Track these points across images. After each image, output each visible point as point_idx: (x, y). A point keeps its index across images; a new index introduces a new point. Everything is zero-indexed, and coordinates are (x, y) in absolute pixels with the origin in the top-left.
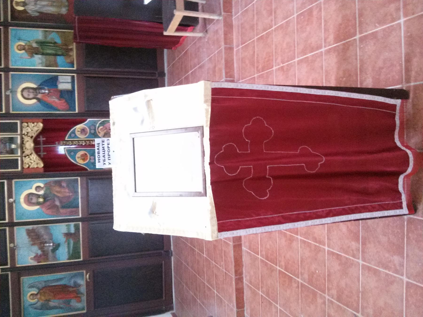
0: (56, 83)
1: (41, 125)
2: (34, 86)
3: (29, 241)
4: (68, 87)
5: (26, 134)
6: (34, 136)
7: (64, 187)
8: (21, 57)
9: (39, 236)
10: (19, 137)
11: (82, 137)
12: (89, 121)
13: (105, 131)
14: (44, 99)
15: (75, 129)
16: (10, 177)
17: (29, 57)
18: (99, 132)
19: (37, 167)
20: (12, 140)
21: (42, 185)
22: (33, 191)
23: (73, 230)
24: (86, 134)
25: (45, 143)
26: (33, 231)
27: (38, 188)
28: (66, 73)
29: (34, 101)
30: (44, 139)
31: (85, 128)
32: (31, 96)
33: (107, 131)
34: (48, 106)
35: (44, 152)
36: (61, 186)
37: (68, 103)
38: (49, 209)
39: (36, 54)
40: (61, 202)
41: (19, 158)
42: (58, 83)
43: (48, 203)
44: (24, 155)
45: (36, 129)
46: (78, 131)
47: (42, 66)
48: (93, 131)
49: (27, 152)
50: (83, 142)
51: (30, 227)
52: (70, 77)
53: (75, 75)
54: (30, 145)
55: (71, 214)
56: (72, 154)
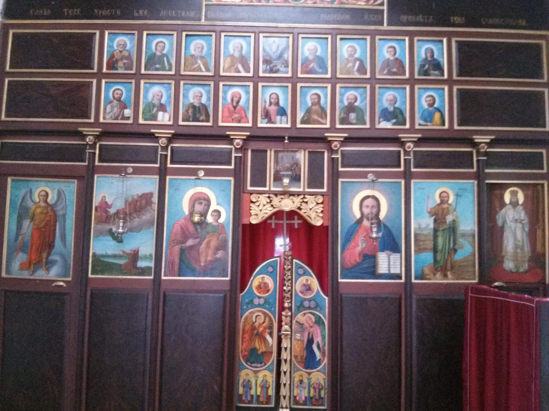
0: (387, 249)
1: (319, 223)
2: (382, 216)
3: (133, 196)
4: (382, 269)
5: (305, 200)
6: (301, 212)
8: (428, 198)
9: (139, 211)
10: (301, 190)
11: (298, 286)
12: (325, 299)
13: (307, 325)
15: (312, 276)
17: (429, 210)
18: (305, 314)
19: (251, 215)
20: (296, 179)
21: (221, 220)
22: (214, 206)
23: (141, 264)
24: (302, 292)
27: (218, 214)
29: (358, 215)
30: (296, 226)
32: (366, 211)
33: (306, 328)
35: (276, 224)
36: (218, 249)
37: (354, 266)
38: (182, 228)
39: (435, 221)
40: (191, 247)
41: (267, 189)
42: (388, 252)
44: (271, 195)
45: (313, 215)
46: (307, 280)
48: (306, 304)
49: (276, 200)
51: (155, 199)
52: (399, 272)
54: (286, 206)
55: (171, 264)
56: (270, 269)
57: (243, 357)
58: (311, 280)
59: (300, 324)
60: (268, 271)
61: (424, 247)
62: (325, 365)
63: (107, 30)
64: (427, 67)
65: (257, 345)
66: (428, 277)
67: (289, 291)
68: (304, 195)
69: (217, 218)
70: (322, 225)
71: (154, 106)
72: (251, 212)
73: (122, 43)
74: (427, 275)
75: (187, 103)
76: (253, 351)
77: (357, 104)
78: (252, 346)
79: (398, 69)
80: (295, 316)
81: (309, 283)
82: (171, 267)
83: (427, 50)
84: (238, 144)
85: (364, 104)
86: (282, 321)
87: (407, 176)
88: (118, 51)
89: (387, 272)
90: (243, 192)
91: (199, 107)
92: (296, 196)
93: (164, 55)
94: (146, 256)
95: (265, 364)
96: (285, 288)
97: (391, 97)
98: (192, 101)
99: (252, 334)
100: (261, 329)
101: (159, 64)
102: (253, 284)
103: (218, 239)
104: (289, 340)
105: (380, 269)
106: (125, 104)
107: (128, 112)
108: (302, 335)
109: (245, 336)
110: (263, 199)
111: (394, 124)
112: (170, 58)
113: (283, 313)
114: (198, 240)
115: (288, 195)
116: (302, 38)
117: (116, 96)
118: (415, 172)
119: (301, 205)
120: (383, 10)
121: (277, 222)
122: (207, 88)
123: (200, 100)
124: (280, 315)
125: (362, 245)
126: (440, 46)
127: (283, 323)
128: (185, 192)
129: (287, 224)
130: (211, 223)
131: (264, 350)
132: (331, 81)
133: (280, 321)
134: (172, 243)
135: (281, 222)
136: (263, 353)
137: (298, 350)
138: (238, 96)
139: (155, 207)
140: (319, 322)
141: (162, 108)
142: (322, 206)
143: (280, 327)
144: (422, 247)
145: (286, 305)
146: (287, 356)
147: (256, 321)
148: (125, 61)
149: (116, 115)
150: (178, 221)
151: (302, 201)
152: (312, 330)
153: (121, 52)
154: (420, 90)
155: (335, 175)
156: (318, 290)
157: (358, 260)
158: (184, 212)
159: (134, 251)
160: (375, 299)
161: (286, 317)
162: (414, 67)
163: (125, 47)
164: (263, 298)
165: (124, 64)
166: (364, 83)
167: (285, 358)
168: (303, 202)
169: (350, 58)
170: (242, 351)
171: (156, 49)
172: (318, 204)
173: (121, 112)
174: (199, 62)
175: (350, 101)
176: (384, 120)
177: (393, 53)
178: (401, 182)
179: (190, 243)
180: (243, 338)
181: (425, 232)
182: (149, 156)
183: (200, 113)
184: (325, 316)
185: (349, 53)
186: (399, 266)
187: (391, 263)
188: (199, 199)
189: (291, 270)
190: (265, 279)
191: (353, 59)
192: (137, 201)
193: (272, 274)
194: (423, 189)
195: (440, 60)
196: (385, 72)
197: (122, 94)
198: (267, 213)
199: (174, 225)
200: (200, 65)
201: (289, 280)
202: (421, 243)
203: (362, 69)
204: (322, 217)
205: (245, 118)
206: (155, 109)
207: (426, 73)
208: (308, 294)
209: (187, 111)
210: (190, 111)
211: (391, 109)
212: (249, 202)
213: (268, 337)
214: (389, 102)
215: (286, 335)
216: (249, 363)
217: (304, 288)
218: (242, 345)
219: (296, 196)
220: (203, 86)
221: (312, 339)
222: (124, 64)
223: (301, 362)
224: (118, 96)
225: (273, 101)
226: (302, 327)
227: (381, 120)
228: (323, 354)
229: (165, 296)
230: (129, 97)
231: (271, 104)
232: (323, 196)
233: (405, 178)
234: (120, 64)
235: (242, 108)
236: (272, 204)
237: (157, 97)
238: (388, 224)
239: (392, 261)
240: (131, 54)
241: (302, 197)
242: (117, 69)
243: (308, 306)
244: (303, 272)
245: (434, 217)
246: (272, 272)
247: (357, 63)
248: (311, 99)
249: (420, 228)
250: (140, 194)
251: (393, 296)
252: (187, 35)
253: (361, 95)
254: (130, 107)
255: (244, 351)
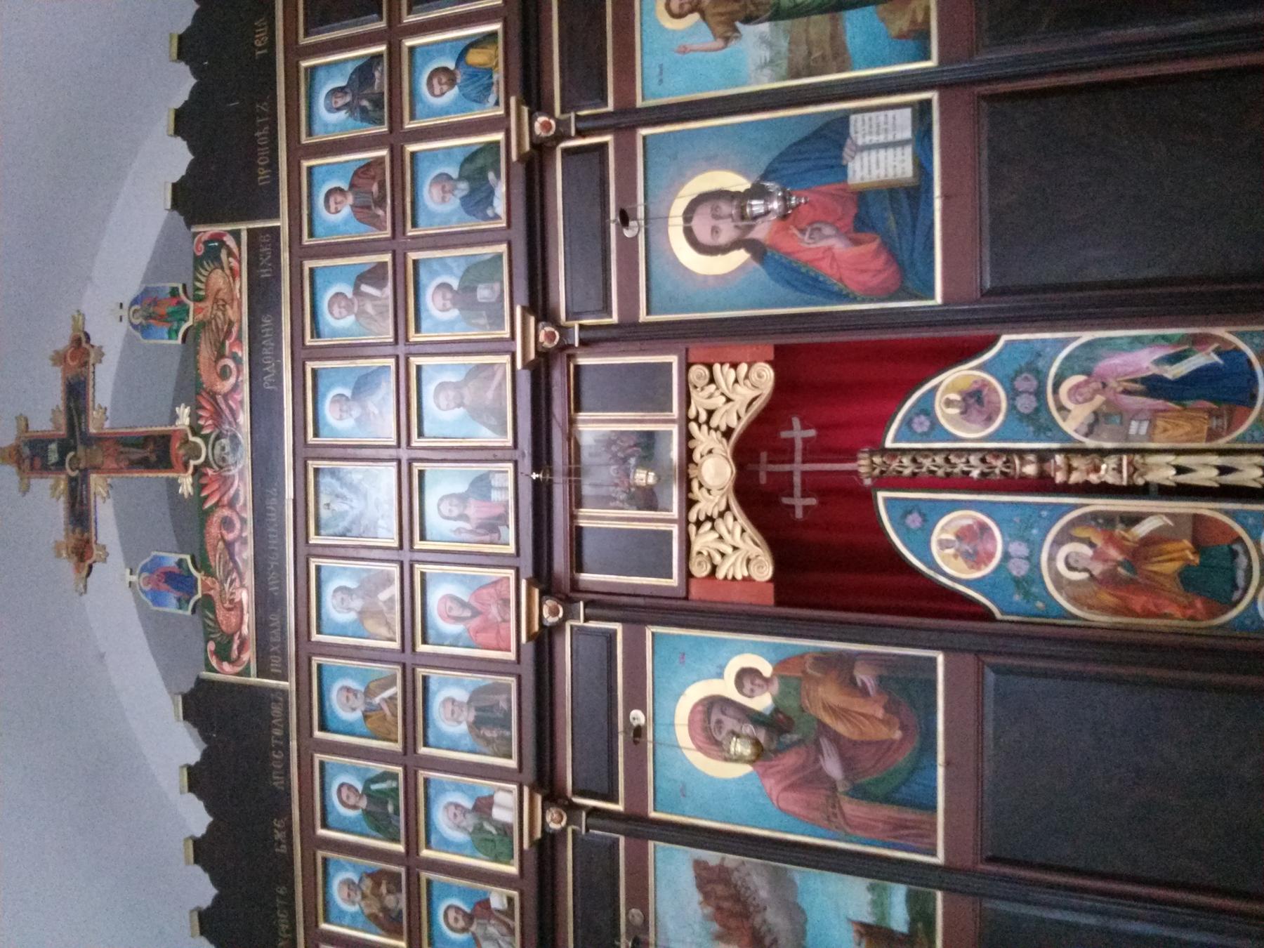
0: (840, 157)
1: (765, 375)
2: (738, 183)
3: (706, 917)
4: (899, 165)
5: (703, 417)
6: (739, 428)
7: (864, 692)
8: (684, 50)
9: (745, 905)
10: (675, 429)
11: (971, 435)
12: (1008, 343)
13: (1099, 399)
14: (786, 245)
15: (935, 388)
16: (641, 610)
17: (720, 43)
18: (1061, 408)
19: (748, 579)
20: (647, 445)
21: (767, 669)
22: (726, 687)
23: (899, 919)
24: (990, 420)
25: (813, 452)
26: (722, 875)
27: (746, 675)
28: (890, 92)
29: (740, 257)
30: (812, 433)
31: (985, 384)
32: (728, 233)
33: (1107, 402)
34: (804, 280)
35: (805, 494)
36: (851, 685)
37: (893, 256)
38: (792, 787)
39: (748, 20)
40: (848, 764)
41: (675, 529)
42: (847, 152)
43: (790, 760)
44: (693, 517)
45: (744, 393)
46: (949, 403)
47: (772, 80)
48: (1026, 404)
49: (707, 504)
50: (974, 459)
51: (712, 857)
52: (907, 112)
53: (933, 95)
54: (718, 473)
55: (899, 833)
56: (914, 521)
57: (1214, 615)
58: (947, 390)
59: (1096, 421)
60: (921, 529)
61: (827, 46)
62: (1230, 332)
63: (317, 926)
64: (365, 103)
65: (1171, 567)
66: (920, 18)
67: (983, 460)
68: (688, 420)
69: (758, 681)
70: (773, 364)
71: (479, 829)
72: (739, 577)
73: (346, 890)
74: (913, 22)
75: (468, 741)
76: (1187, 578)
77: (455, 284)
78: (1175, 587)
79: (373, 178)
80: (1070, 439)
81: (955, 397)
82: (906, 832)
83: (331, 110)
84: (554, 612)
85: (454, 265)
86: (1087, 483)
87: (628, 119)
88: (363, 904)
89: (908, 150)
90: (686, 598)
91: (478, 709)
92: (692, 444)
93: (367, 792)
94: (874, 903)
95: (1239, 540)
96: (975, 474)
97: (436, 192)
98: (464, 728)
99: (1129, 584)
100: (1114, 554)
101: (387, 803)
102: (964, 576)
103: (818, 682)
104: (1152, 459)
105: (899, 175)
106: (479, 903)
107: (498, 899)
108: (1136, 415)
109: (1138, 608)
110: (704, 541)
111: (498, 176)
112: (371, 775)
113: (1059, 478)
114: (824, 743)
115: (691, 466)
116: (316, 435)
117: (461, 924)
118: (616, 100)
119: (717, 429)
120: (249, 231)
121: (797, 490)
122: (433, 686)
123: (460, 705)
124: (1066, 489)
125: (828, 237)
126: (321, 74)
127: (1094, 478)
128: (691, 770)
129: (804, 462)
130: (775, 700)
131: (1187, 543)
132: (399, 252)
133: (1086, 489)
134: (832, 818)
135: (797, 480)
136: (1198, 547)
137: (1187, 428)
138: (449, 604)
139: (731, 860)
140: (1082, 362)
141: (483, 806)
142: (717, 367)
143: (1105, 490)
144: (828, 51)
145: (1030, 470)
146: (1206, 465)
147: (1086, 570)
148: (383, 889)
149: (505, 930)
150: (769, 796)
151: (705, 428)
152: (1112, 383)
153: (364, 897)
154: (418, 113)
155: (631, 334)
156: (979, 368)
157: (874, 246)
158: (746, 777)
159: (861, 935)
160: (996, 181)
161: (1070, 469)
162: (367, 137)
163: (353, 883)
164: (1006, 544)
165: (389, 892)
166: (403, 161)
167: (1215, 472)
168: (707, 422)
169: (356, 309)
170: (1192, 618)
171: (354, 807)
172: (712, 380)
173: (497, 919)
174: (377, 700)
175: (449, 304)
176: (491, 204)
177: (339, 198)
178: (645, 138)
179: (832, 767)
180: (1148, 614)
181: (784, 44)
182: (599, 865)
183: (492, 707)
184: (1065, 342)
185: (344, 312)
186: (891, 113)
187: (882, 139)
188: (706, 729)
189: (915, 454)
190: (945, 536)
191: (356, 301)
192: (719, 908)
193: (931, 514)
194: (661, 67)
195: (350, 68)
196: (380, 212)
197: (458, 909)
198: (743, 531)
199: (780, 808)
200: (385, 700)
201: (947, 460)
202: (817, 54)
203: (374, 276)
204: (750, 365)
205: (498, 587)
206: (488, 827)
207: (378, 104)
208: (993, 398)
209: (489, 742)
210: (488, 734)
211: (464, 187)
212: (709, 582)
213: (1142, 529)
214: (448, 196)
215: (1134, 469)
216: (1236, 595)
217: (974, 413)
218: (1165, 616)
219: (692, 444)
220: (430, 695)
221: (1144, 380)
222: (389, 892)
223: (1231, 412)
224: (460, 918)
225: (456, 512)
226: (1107, 416)
227: (490, 212)
228: (1199, 341)
229: (992, 860)
230: (462, 893)
231: (463, 517)
232: (689, 366)
233: (633, 128)
234: (390, 901)
235: (476, 594)
236: (715, 515)
237: (460, 818)
238: (765, 161)
239: (875, 139)
240: (369, 871)
241: (693, 426)
242: (400, 912)
243: (1033, 398)
244: (923, 418)
245: (738, 24)
246: (923, 515)
247: (365, 288)
248: (448, 408)
249: (771, 63)
250: (697, 897)
251: (985, 121)
252: (323, 727)
253: (434, 274)
254: (485, 893)
255: (1190, 612)
